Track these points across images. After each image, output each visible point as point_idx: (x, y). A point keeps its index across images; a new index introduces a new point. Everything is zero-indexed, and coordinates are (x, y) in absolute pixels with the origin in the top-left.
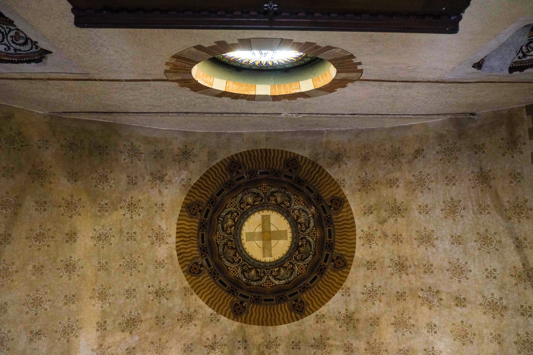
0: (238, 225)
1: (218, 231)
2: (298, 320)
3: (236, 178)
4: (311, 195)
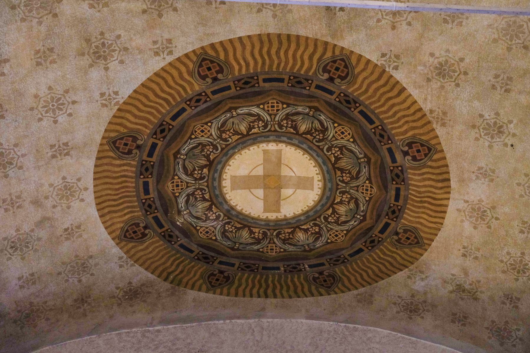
0: (326, 203)
1: (367, 201)
2: (212, 46)
3: (324, 267)
4: (184, 241)
